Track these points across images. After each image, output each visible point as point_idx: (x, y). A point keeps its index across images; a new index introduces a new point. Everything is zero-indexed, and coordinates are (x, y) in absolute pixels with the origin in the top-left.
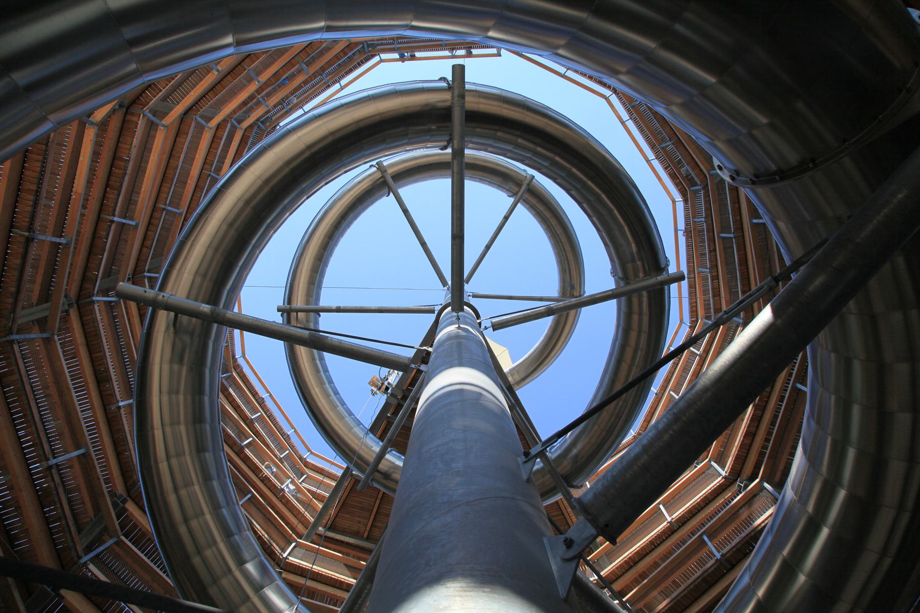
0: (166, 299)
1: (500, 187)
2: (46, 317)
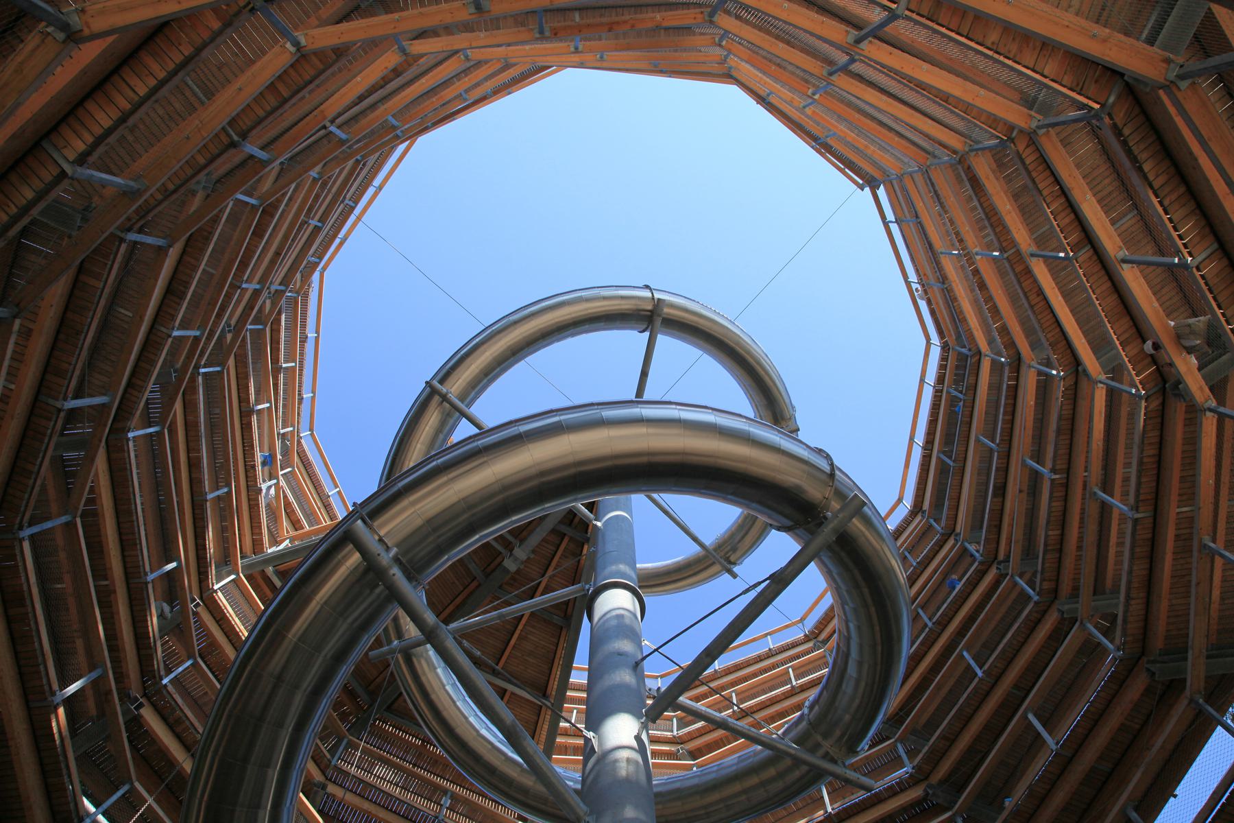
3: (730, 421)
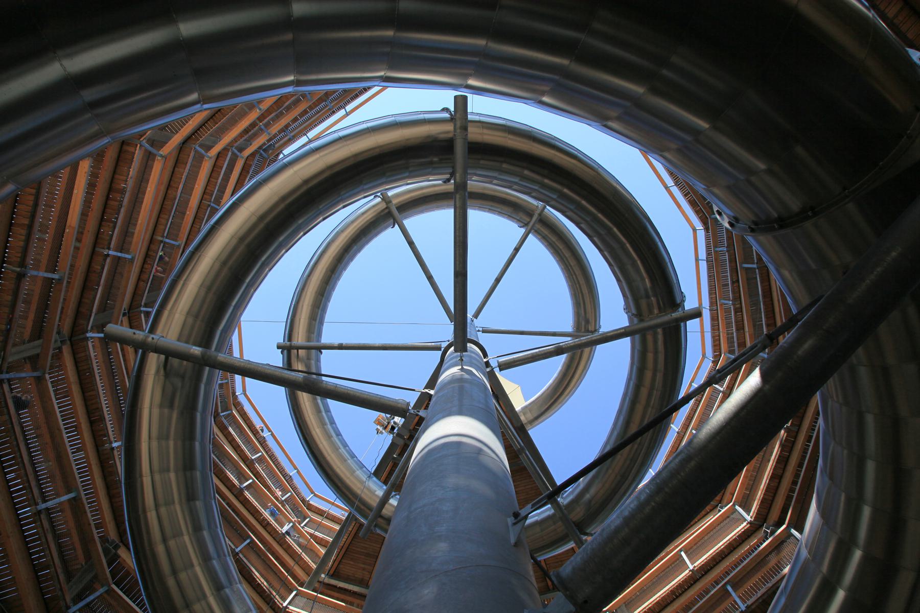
0: (155, 341)
1: (510, 217)
2: (38, 355)
3: (354, 128)
